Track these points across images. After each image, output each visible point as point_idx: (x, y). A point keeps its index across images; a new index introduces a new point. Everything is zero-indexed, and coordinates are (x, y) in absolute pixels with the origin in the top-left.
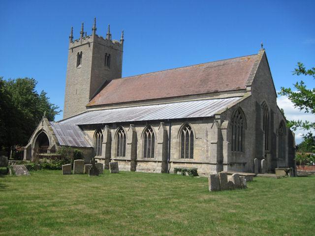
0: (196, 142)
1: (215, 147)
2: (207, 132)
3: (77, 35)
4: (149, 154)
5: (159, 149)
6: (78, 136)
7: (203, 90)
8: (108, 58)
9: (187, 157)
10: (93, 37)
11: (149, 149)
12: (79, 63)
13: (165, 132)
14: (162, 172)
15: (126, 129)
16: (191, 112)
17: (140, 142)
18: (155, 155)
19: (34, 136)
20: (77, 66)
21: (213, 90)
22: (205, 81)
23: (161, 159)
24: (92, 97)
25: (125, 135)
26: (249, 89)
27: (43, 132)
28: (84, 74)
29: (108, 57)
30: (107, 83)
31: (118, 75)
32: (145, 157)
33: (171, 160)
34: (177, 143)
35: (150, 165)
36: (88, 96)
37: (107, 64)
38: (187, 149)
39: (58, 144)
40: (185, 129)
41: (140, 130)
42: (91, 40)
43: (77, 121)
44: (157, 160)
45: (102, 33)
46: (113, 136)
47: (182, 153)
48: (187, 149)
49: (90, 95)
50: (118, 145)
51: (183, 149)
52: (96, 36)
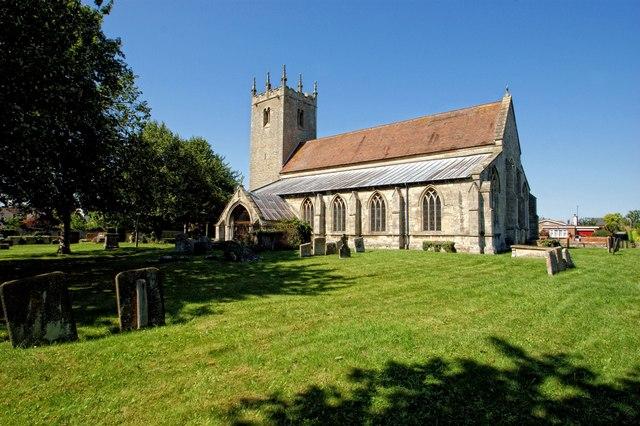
0: (445, 210)
1: (476, 215)
2: (460, 196)
3: (261, 86)
5: (393, 221)
8: (301, 114)
9: (432, 229)
13: (402, 198)
14: (401, 248)
15: (313, 199)
17: (366, 212)
19: (228, 209)
21: (449, 146)
22: (434, 137)
23: (397, 232)
28: (271, 137)
29: (302, 114)
30: (301, 145)
31: (313, 136)
32: (373, 230)
34: (417, 212)
35: (381, 240)
36: (280, 162)
37: (301, 120)
38: (432, 215)
39: (263, 218)
40: (428, 194)
42: (281, 93)
43: (275, 189)
44: (390, 233)
45: (294, 85)
46: (328, 206)
47: (425, 224)
49: (284, 161)
50: (335, 217)
51: (425, 219)
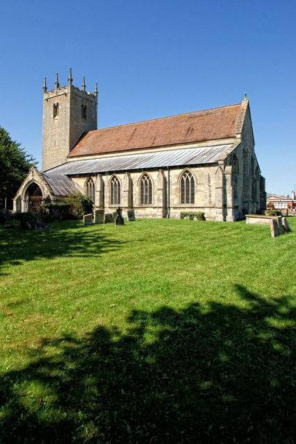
0: (197, 188)
2: (209, 177)
4: (188, 199)
5: (157, 196)
6: (67, 183)
7: (99, 150)
8: (84, 109)
9: (188, 202)
10: (69, 87)
11: (146, 196)
12: (55, 114)
15: (94, 179)
16: (187, 159)
17: (136, 189)
18: (153, 202)
19: (23, 187)
20: (55, 116)
21: (201, 138)
23: (161, 204)
24: (71, 149)
25: (150, 184)
26: (239, 136)
27: (34, 183)
28: (60, 128)
30: (84, 134)
31: (94, 126)
32: (142, 203)
33: (171, 206)
34: (176, 189)
35: (148, 211)
36: (68, 148)
37: (84, 115)
38: (188, 193)
39: (53, 194)
40: (185, 175)
41: (106, 179)
44: (156, 205)
45: (78, 84)
46: (106, 184)
47: (183, 199)
48: (188, 194)
51: (183, 195)
52: (72, 87)
